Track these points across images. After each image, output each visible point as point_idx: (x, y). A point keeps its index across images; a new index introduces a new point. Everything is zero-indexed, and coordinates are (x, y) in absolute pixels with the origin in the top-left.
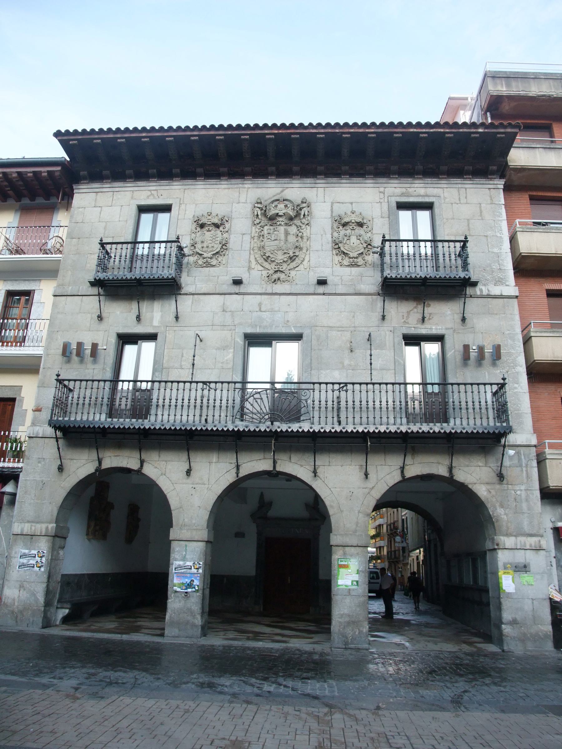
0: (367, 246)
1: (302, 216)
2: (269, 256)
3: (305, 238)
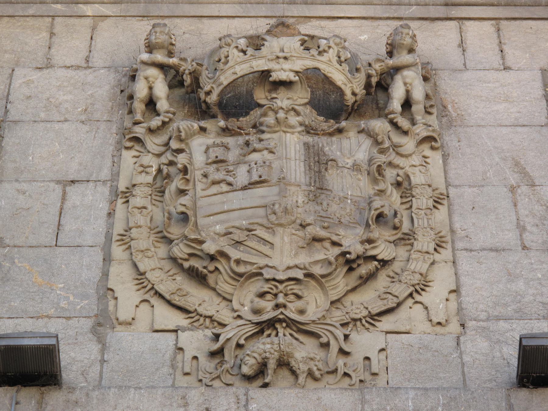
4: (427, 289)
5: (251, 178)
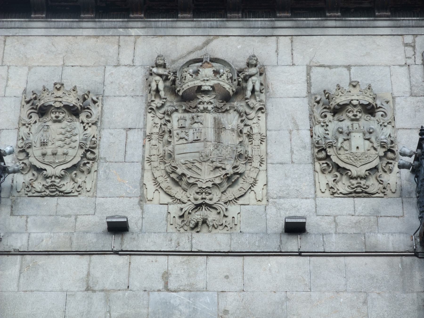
0: (385, 153)
1: (249, 93)
2: (183, 175)
5: (194, 138)
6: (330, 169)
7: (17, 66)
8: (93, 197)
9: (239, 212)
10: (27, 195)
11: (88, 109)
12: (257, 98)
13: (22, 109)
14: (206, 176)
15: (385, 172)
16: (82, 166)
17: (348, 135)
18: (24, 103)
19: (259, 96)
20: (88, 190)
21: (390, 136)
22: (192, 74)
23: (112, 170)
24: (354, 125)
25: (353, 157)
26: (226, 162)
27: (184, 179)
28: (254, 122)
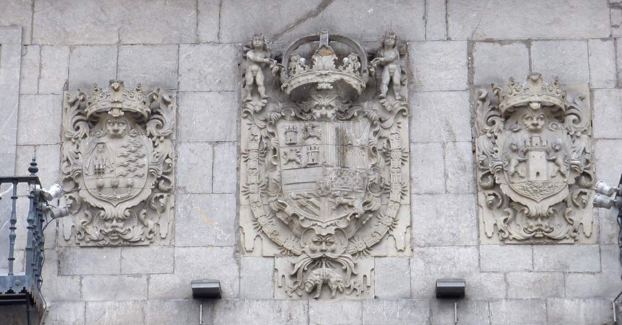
0: (577, 180)
1: (384, 89)
2: (295, 216)
3: (396, 156)
4: (396, 226)
6: (499, 204)
7: (52, 46)
8: (169, 247)
9: (373, 267)
10: (78, 245)
11: (158, 113)
12: (397, 94)
13: (64, 114)
14: (327, 219)
15: (577, 206)
16: (153, 202)
17: (525, 154)
18: (66, 105)
19: (398, 91)
20: (163, 236)
21: (584, 151)
22: (304, 66)
23: (196, 206)
24: (534, 139)
25: (531, 188)
26: (353, 196)
27: (296, 222)
28: (393, 132)
